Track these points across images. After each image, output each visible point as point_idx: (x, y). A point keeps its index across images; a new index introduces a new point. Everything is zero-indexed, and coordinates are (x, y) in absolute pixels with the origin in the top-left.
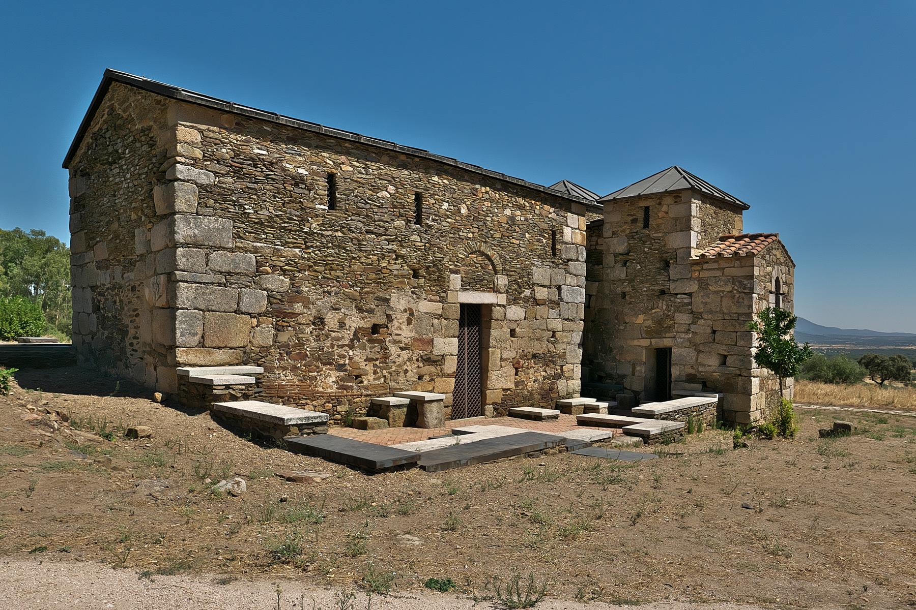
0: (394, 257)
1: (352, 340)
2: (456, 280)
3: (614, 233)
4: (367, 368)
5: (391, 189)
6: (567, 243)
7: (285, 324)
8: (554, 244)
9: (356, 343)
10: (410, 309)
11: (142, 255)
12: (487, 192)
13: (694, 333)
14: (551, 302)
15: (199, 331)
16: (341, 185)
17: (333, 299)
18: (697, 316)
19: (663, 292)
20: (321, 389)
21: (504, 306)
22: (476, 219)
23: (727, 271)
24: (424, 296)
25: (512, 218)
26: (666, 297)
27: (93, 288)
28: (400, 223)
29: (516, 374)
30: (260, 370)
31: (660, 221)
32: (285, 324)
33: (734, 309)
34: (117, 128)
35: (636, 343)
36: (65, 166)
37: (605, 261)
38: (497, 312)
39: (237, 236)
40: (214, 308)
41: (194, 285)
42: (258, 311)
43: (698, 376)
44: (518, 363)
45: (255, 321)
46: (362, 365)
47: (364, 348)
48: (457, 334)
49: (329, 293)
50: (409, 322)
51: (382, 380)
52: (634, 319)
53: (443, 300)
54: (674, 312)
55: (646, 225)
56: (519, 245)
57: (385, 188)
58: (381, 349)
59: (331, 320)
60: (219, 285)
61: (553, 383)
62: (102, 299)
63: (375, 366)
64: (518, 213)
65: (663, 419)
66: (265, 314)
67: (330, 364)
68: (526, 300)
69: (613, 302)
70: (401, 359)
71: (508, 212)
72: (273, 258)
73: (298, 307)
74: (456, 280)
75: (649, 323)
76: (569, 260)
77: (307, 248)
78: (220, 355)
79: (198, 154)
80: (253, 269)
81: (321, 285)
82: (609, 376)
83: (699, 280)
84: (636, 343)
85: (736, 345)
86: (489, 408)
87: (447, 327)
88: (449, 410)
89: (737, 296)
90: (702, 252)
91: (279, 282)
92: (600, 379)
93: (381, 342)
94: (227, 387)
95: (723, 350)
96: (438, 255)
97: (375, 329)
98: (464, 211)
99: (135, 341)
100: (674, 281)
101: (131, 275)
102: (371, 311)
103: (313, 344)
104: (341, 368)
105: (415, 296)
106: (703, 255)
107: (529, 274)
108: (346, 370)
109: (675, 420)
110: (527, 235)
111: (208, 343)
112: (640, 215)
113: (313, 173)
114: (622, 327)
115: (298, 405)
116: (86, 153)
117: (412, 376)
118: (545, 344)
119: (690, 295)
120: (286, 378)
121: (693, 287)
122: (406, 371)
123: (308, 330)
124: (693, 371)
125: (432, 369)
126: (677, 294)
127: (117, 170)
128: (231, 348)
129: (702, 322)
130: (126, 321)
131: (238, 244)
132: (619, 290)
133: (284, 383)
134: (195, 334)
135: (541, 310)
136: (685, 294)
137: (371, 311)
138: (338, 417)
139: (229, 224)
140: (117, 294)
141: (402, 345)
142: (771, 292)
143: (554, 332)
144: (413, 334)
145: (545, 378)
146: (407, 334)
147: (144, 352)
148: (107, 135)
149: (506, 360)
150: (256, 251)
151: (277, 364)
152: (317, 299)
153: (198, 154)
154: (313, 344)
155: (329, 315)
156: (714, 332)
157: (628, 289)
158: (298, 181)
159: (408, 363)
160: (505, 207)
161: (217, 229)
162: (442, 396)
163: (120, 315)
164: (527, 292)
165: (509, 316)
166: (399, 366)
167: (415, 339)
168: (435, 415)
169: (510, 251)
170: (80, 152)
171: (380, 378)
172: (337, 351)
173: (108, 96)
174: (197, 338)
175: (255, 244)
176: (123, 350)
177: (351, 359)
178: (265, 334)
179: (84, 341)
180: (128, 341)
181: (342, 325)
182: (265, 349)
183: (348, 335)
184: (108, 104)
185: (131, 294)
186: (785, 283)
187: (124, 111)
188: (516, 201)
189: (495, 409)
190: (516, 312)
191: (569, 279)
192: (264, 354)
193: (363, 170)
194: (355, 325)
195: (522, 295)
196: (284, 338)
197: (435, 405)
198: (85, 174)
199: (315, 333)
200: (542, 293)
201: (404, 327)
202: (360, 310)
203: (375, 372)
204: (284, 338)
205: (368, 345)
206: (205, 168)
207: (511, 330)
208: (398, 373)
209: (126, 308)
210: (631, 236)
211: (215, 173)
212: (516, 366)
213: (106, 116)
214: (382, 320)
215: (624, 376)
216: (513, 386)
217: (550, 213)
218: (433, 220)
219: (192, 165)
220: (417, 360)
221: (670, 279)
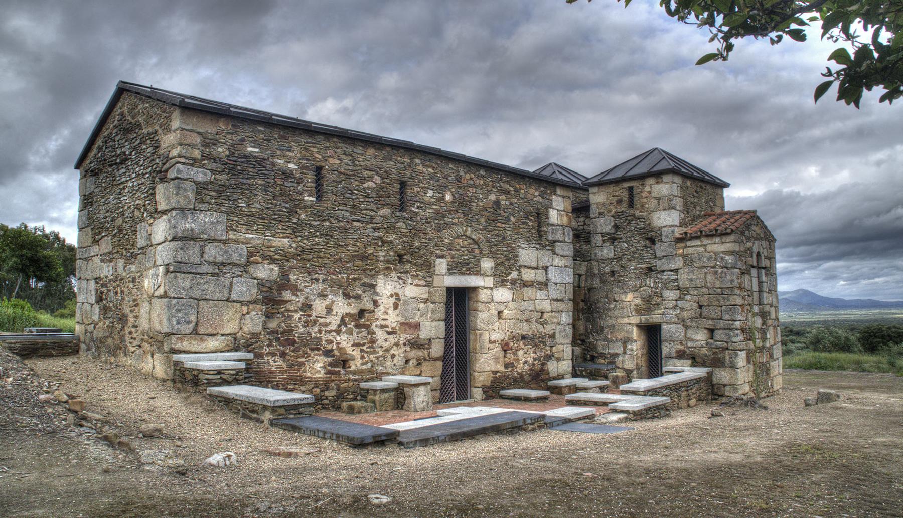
0: (380, 244)
1: (339, 326)
2: (441, 265)
3: (600, 213)
4: (354, 353)
5: (378, 179)
6: (553, 225)
7: (274, 311)
8: (539, 226)
9: (344, 329)
10: (397, 295)
11: (142, 248)
12: (471, 179)
13: (682, 309)
14: (540, 283)
15: (193, 318)
16: (329, 177)
17: (321, 286)
18: (683, 292)
19: (650, 269)
20: (309, 374)
21: (491, 289)
22: (461, 204)
23: (709, 248)
24: (410, 281)
25: (497, 203)
26: (653, 274)
27: (97, 280)
28: (386, 211)
29: (505, 357)
30: (251, 356)
31: (645, 200)
32: (274, 311)
33: (718, 285)
34: (127, 131)
35: (626, 320)
36: (78, 167)
37: (594, 241)
38: (483, 295)
39: (230, 228)
40: (208, 297)
41: (191, 275)
42: (248, 299)
43: (688, 352)
44: (507, 344)
45: (245, 309)
46: (349, 350)
47: (350, 333)
48: (443, 317)
49: (317, 280)
50: (396, 307)
51: (369, 365)
52: (623, 297)
53: (429, 285)
54: (662, 289)
55: (631, 204)
56: (504, 228)
57: (370, 178)
58: (368, 334)
59: (319, 306)
60: (213, 275)
61: (543, 364)
62: (104, 290)
63: (362, 351)
64: (504, 197)
65: (651, 395)
66: (255, 302)
67: (318, 349)
68: (513, 282)
69: (602, 281)
70: (388, 343)
71: (493, 197)
72: (264, 249)
73: (287, 295)
74: (441, 265)
75: (638, 301)
76: (555, 242)
77: (297, 237)
78: (212, 343)
79: (197, 154)
80: (243, 261)
81: (309, 273)
82: (602, 355)
83: (684, 256)
84: (626, 320)
85: (721, 319)
86: (478, 393)
87: (433, 312)
88: (438, 394)
89: (720, 271)
90: (685, 230)
91: (266, 272)
92: (593, 358)
93: (367, 327)
94: (219, 372)
95: (709, 323)
96: (424, 240)
97: (362, 313)
98: (448, 197)
99: (133, 330)
100: (660, 259)
101: (133, 268)
102: (358, 297)
103: (302, 330)
104: (328, 353)
105: (401, 282)
106: (686, 233)
107: (516, 256)
108: (333, 356)
109: (664, 395)
110: (512, 218)
111: (202, 330)
112: (625, 195)
113: (303, 167)
114: (612, 306)
115: (286, 389)
116: (96, 155)
117: (399, 360)
118: (534, 326)
119: (676, 271)
120: (274, 364)
121: (679, 263)
122: (393, 356)
123: (297, 316)
124: (682, 347)
125: (420, 353)
126: (663, 271)
127: (124, 170)
128: (223, 335)
129: (688, 298)
130: (127, 311)
131: (231, 236)
132: (607, 270)
133: (273, 369)
134: (189, 323)
135: (529, 292)
136: (672, 271)
137: (358, 297)
138: (326, 402)
139: (223, 218)
140: (118, 286)
141: (389, 330)
142: (753, 267)
143: (542, 313)
144: (399, 319)
145: (535, 359)
146: (393, 319)
147: (142, 340)
148: (117, 139)
149: (494, 342)
150: (247, 242)
151: (266, 350)
152: (305, 287)
153: (197, 154)
154: (302, 330)
155: (317, 301)
156: (701, 307)
157: (617, 268)
158: (287, 175)
159: (395, 348)
160: (490, 192)
161: (212, 223)
162: (430, 380)
163: (120, 305)
164: (514, 275)
165: (496, 299)
166: (387, 350)
167: (402, 324)
168: (420, 399)
169: (497, 235)
170: (92, 155)
171: (366, 363)
172: (324, 337)
173: (120, 104)
174: (191, 326)
175: (247, 236)
176: (122, 339)
177: (338, 344)
178: (254, 322)
179: (86, 330)
180: (127, 331)
181: (329, 310)
182: (256, 336)
183: (334, 322)
184: (119, 111)
185: (131, 285)
186: (766, 258)
187: (133, 119)
188: (501, 186)
189: (484, 392)
190: (503, 294)
191: (557, 261)
192: (254, 341)
193: (350, 163)
194: (342, 310)
195: (509, 278)
196: (273, 325)
197: (422, 388)
198: (95, 173)
199: (303, 319)
200: (528, 275)
201: (390, 312)
202: (347, 296)
203: (362, 357)
204: (273, 325)
205: (355, 331)
206: (203, 166)
207: (499, 313)
208: (385, 357)
209: (127, 299)
210: (617, 216)
211: (211, 170)
212: (506, 348)
213: (116, 122)
214: (369, 306)
215: (617, 355)
216: (501, 368)
217: (535, 197)
218: (418, 207)
219: (191, 165)
220: (405, 344)
221: (656, 257)
